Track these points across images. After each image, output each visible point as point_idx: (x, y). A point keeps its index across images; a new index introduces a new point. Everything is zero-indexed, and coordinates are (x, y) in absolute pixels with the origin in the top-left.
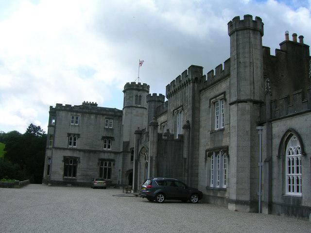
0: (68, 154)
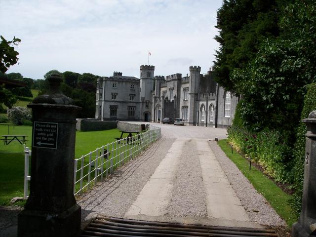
0: (113, 104)
